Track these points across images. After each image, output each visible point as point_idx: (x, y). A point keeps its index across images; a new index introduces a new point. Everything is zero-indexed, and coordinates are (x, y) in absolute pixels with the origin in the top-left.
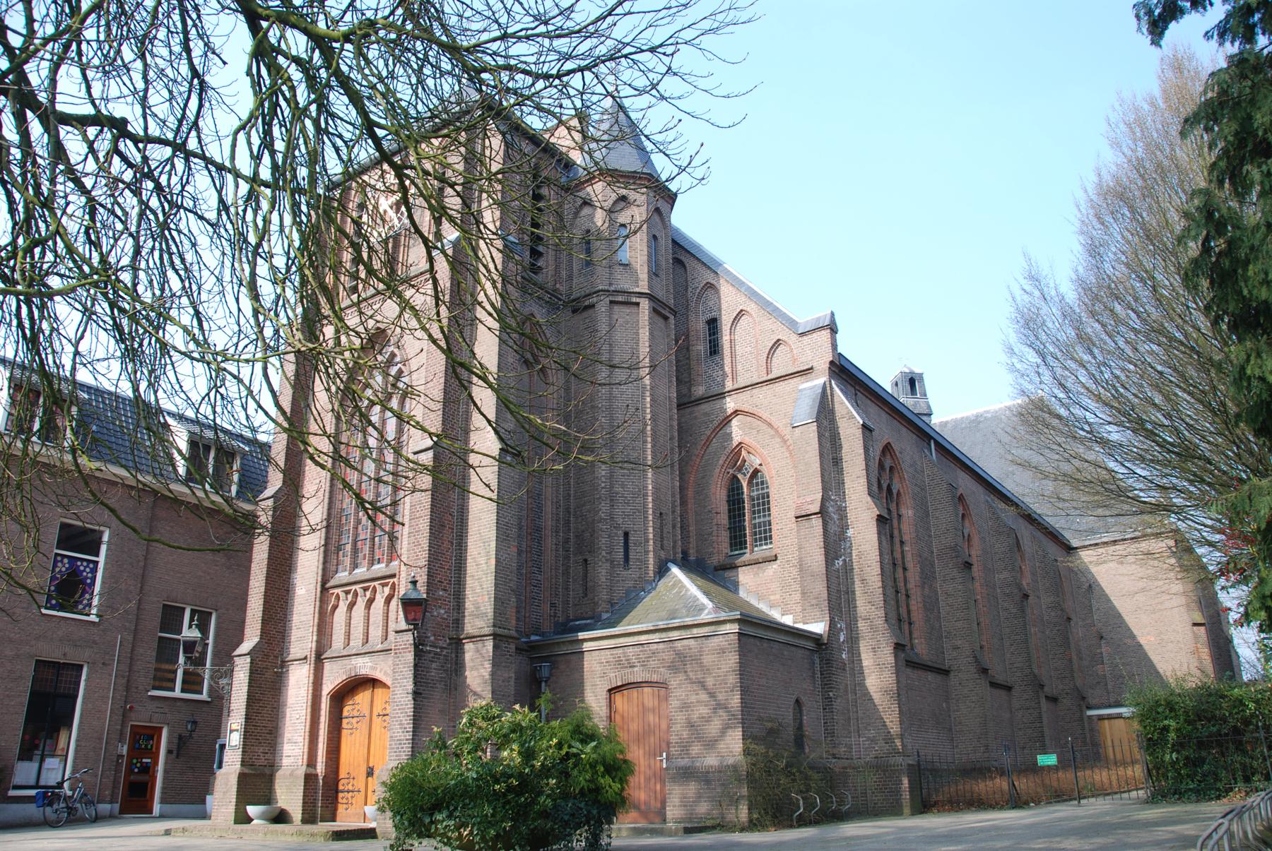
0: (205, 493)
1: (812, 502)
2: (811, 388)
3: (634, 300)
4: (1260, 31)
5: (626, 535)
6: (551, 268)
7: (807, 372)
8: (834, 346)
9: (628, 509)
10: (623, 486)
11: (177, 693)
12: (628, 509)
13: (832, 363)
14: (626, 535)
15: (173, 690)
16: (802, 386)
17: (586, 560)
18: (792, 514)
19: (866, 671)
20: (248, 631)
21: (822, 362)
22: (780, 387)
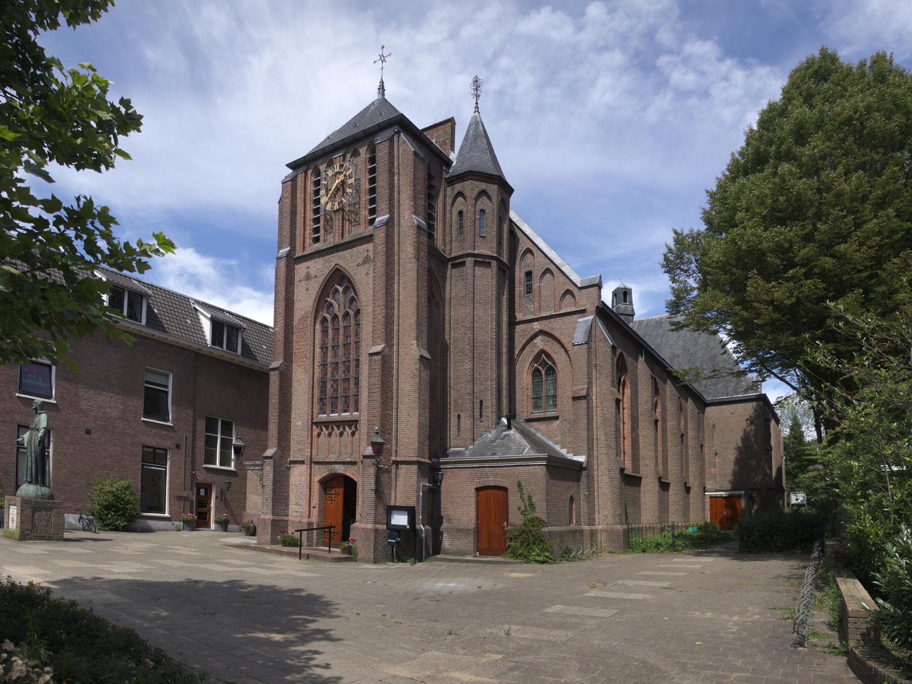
0: (222, 351)
1: (582, 389)
2: (585, 321)
3: (460, 260)
4: (71, 182)
5: (481, 402)
6: (308, 232)
7: (583, 312)
8: (600, 296)
9: (482, 388)
10: (480, 374)
11: (218, 466)
12: (482, 388)
13: (597, 307)
14: (481, 402)
15: (215, 463)
16: (579, 320)
17: (459, 416)
18: (570, 394)
19: (282, 355)
20: (270, 443)
21: (591, 308)
22: (566, 319)
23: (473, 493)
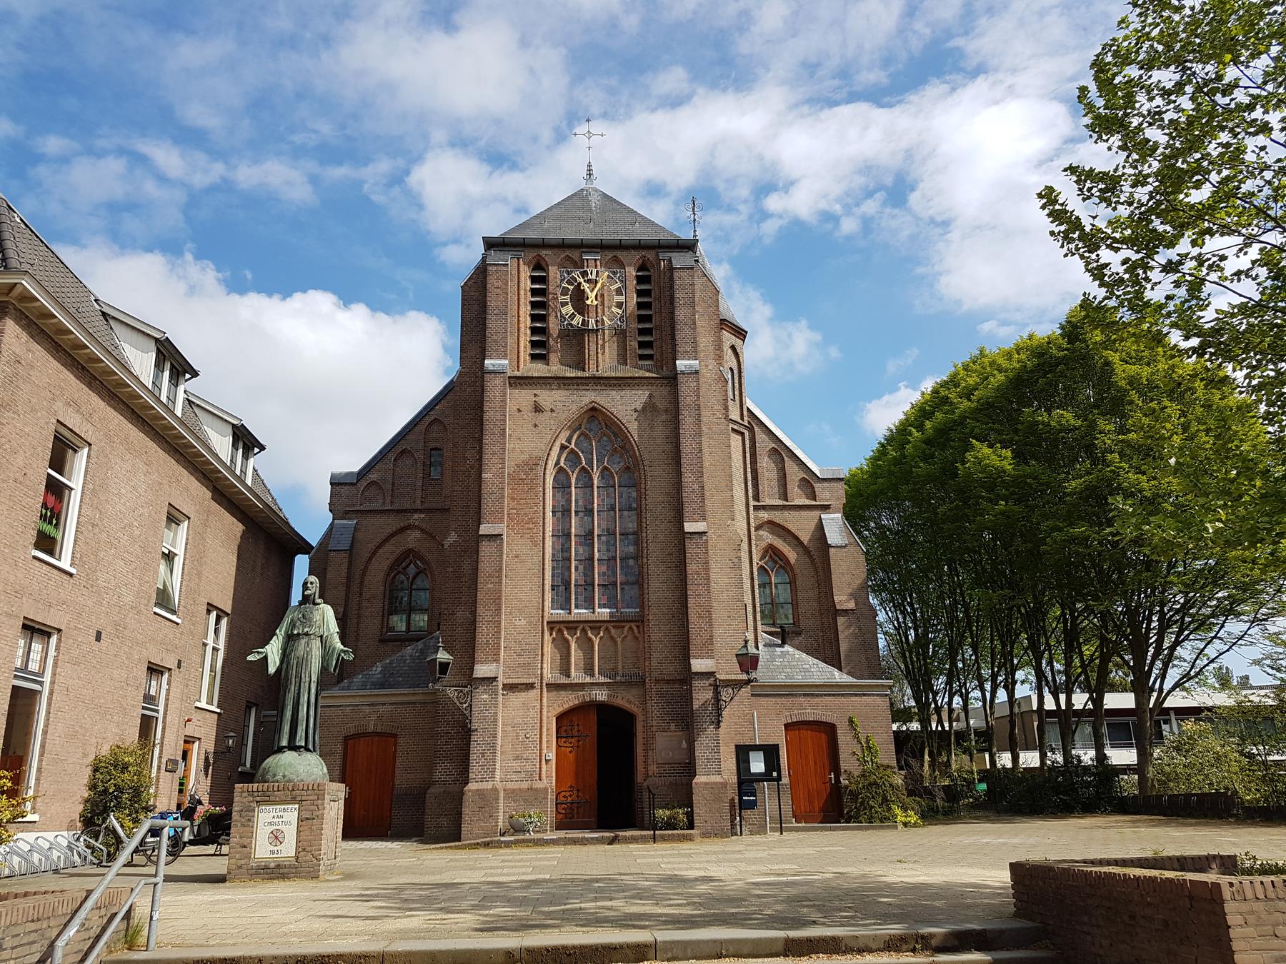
23: (849, 714)
